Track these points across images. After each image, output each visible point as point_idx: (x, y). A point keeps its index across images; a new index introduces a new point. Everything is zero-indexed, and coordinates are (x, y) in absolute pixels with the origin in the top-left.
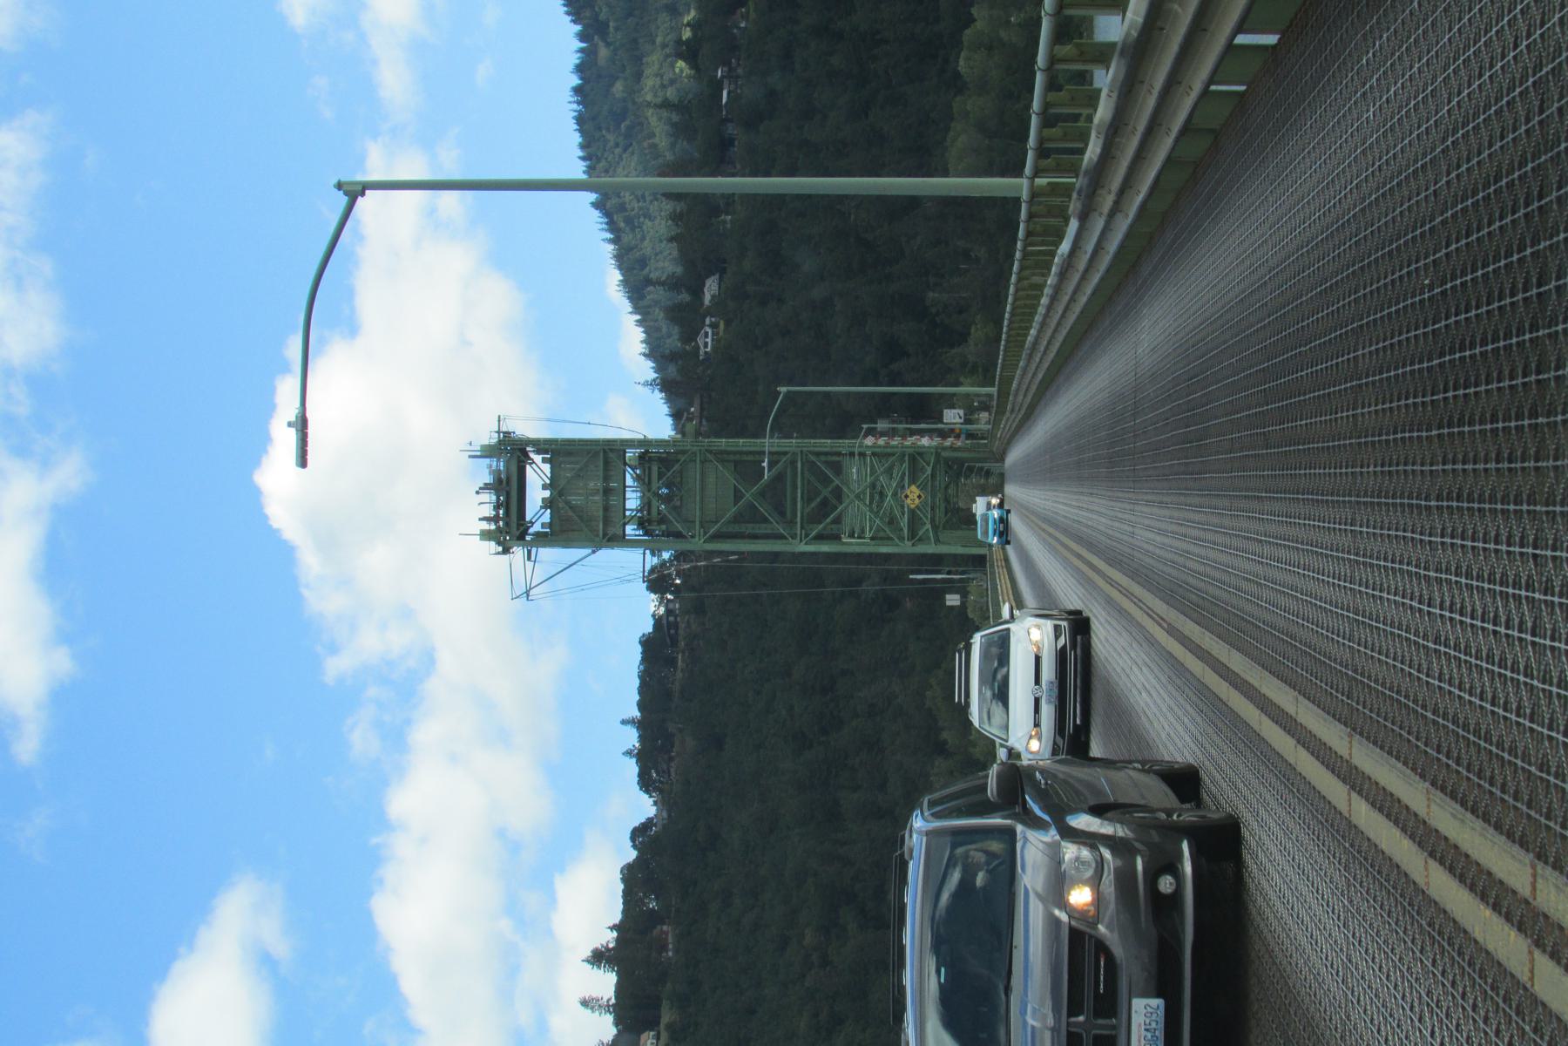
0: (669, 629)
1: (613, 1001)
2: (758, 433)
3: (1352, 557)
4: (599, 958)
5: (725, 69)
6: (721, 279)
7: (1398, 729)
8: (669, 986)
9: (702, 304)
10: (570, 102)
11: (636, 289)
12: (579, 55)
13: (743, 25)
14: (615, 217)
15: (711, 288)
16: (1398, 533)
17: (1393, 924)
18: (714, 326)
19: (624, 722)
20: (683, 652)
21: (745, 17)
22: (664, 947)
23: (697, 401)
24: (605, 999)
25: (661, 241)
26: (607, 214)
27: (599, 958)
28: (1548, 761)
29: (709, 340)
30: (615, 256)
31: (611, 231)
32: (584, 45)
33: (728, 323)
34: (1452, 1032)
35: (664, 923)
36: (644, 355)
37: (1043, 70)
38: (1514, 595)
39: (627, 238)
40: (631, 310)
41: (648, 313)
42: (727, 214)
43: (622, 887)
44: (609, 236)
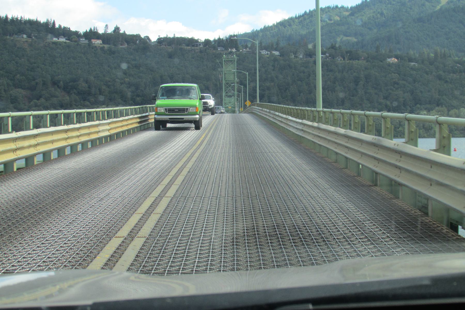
0: (196, 44)
1: (107, 32)
2: (237, 92)
3: (216, 213)
4: (117, 29)
5: (328, 56)
6: (278, 55)
7: (164, 226)
8: (113, 46)
9: (273, 51)
10: (333, 5)
11: (283, 24)
12: (347, 7)
13: (339, 60)
14: (302, 17)
15: (277, 53)
16: (224, 233)
17: (106, 224)
18: (268, 54)
19: (174, 34)
20: (191, 48)
21: (341, 60)
22: (122, 45)
23: (250, 50)
24: (108, 30)
25: (296, 30)
26: (303, 15)
27: (117, 29)
28: (164, 257)
29: (264, 53)
30: (292, 17)
31: (299, 16)
32: (349, 8)
33: (268, 58)
34: (73, 243)
35: (127, 45)
36: (265, 26)
37: (437, 119)
38: (209, 255)
39: (297, 20)
40: (277, 22)
41: (276, 27)
42: (294, 56)
43: (135, 34)
44: (297, 16)
